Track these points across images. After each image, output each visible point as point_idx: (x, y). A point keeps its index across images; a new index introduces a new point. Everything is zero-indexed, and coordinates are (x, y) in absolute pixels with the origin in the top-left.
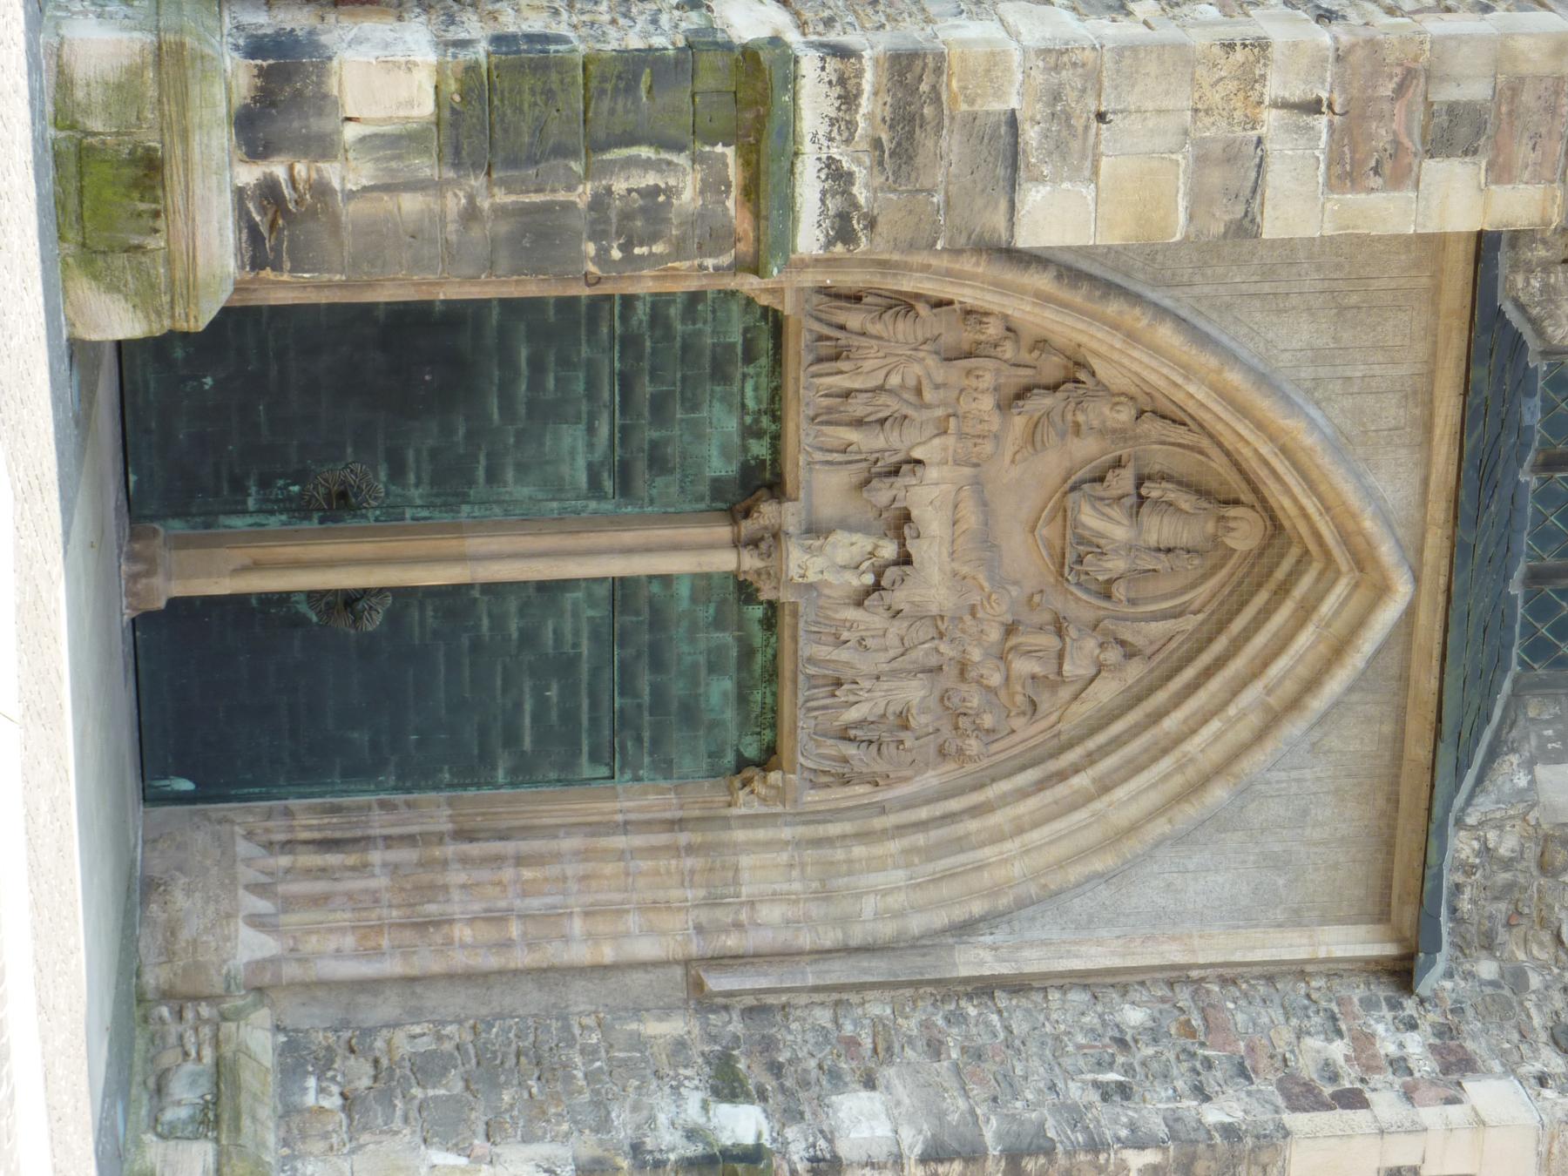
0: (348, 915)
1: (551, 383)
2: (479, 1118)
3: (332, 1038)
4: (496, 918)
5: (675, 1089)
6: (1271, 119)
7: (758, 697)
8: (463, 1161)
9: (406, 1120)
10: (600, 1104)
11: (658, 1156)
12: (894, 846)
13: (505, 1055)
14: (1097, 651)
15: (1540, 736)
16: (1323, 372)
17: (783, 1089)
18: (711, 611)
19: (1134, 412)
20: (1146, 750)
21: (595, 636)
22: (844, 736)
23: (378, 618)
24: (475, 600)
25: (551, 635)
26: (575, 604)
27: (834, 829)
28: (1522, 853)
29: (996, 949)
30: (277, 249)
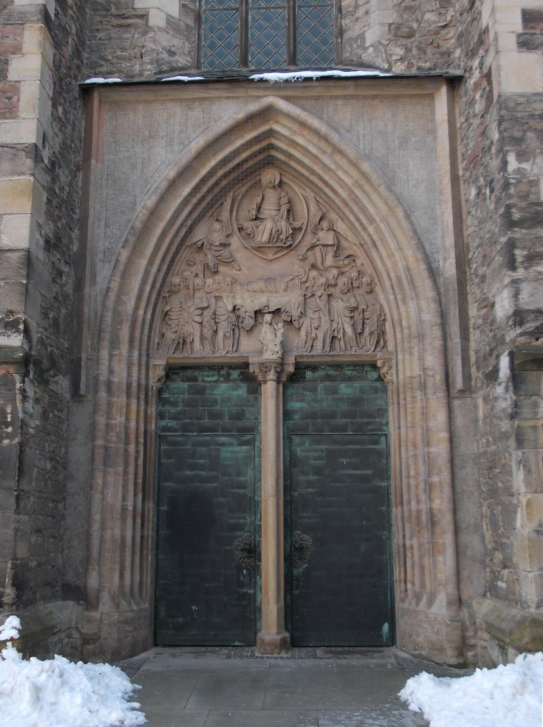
3: (488, 570)
12: (402, 309)
14: (324, 231)
15: (356, 49)
16: (176, 141)
18: (308, 393)
19: (216, 223)
21: (318, 443)
23: (306, 537)
24: (299, 494)
25: (317, 462)
26: (303, 451)
28: (402, 45)
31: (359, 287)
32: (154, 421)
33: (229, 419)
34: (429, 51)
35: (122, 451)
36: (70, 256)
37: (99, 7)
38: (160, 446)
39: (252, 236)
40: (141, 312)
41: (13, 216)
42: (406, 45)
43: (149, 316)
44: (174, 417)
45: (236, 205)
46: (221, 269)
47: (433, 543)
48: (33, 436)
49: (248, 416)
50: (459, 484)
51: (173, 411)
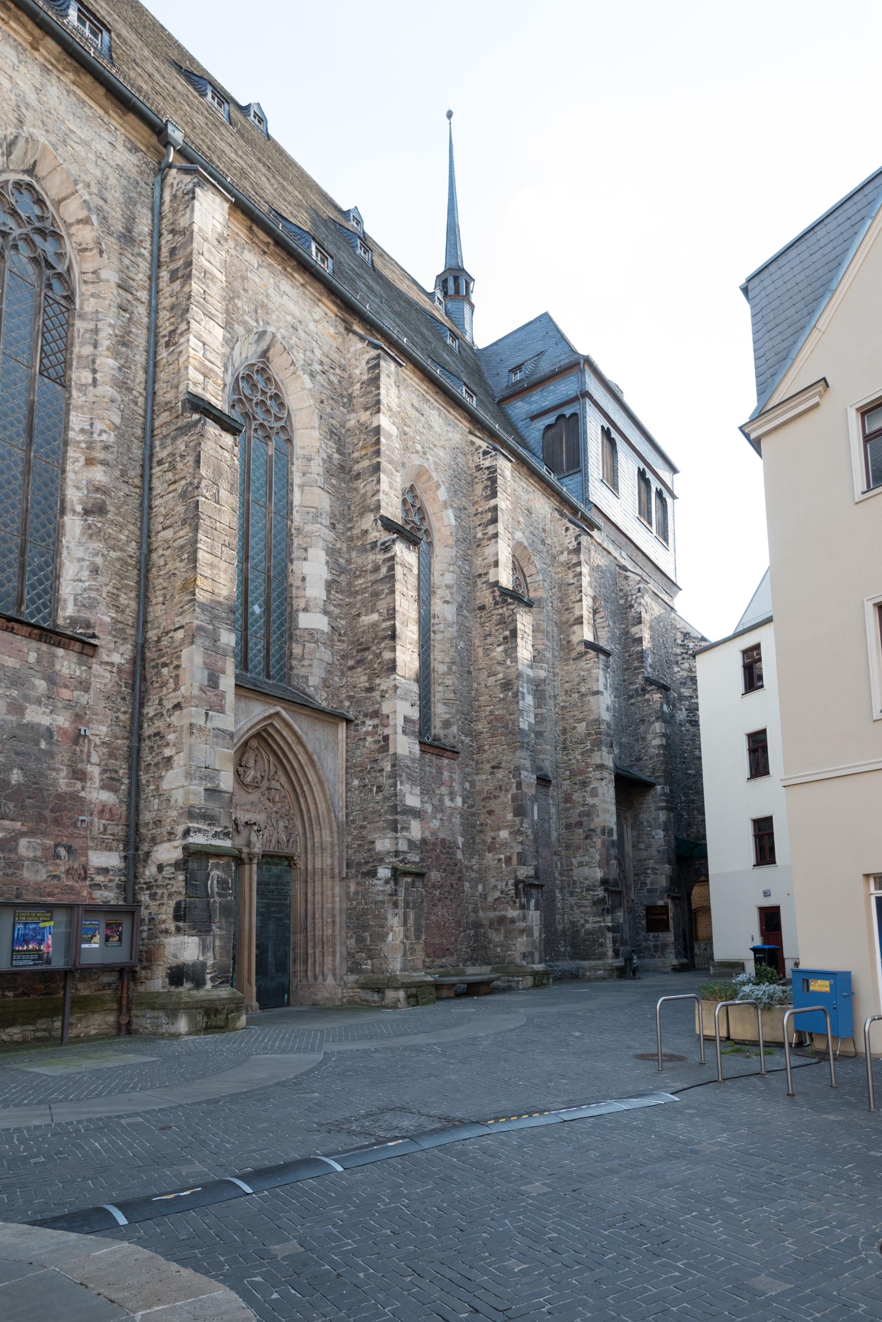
2: (377, 930)
6: (209, 725)
8: (391, 934)
10: (376, 903)
22: (288, 841)
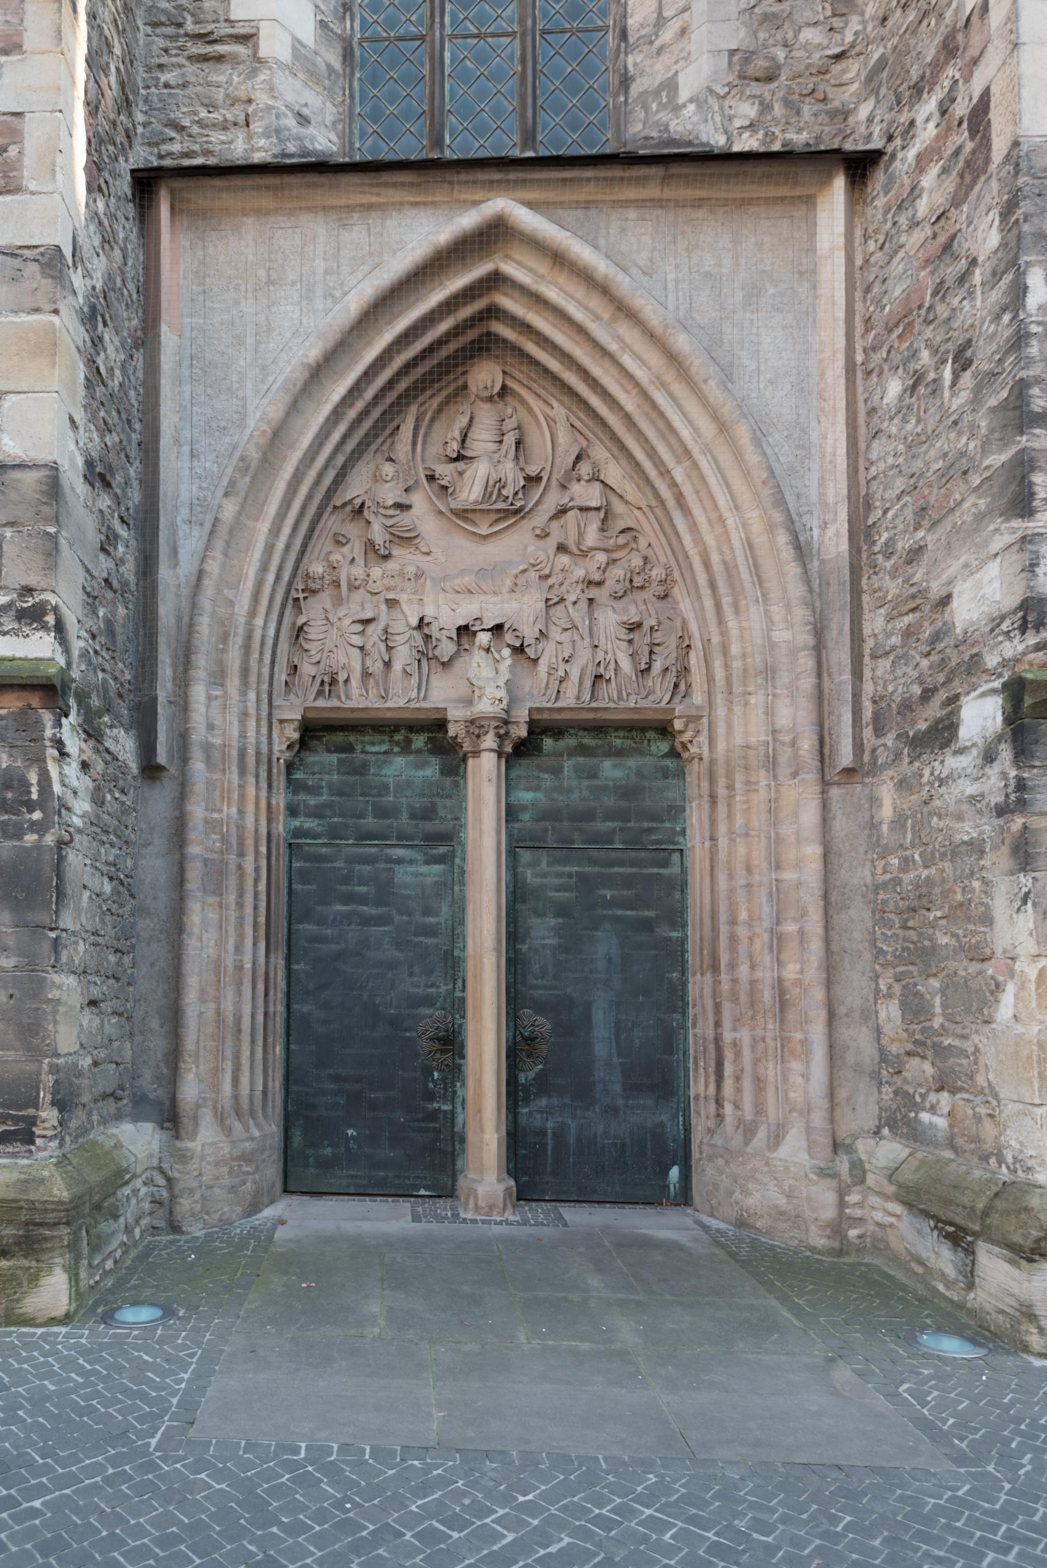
0: (771, 1065)
1: (363, 889)
3: (887, 1090)
4: (778, 943)
5: (942, 782)
7: (619, 741)
8: (1010, 988)
9: (964, 1037)
10: (954, 851)
11: (1010, 789)
12: (732, 623)
13: (906, 939)
14: (583, 483)
15: (657, 112)
16: (319, 292)
17: (948, 681)
18: (546, 776)
19: (388, 463)
20: (653, 422)
23: (541, 1020)
26: (535, 875)
27: (719, 673)
28: (755, 97)
29: (826, 524)
30: (17, 1119)
31: (642, 588)
32: (281, 818)
33: (410, 818)
34: (807, 110)
35: (232, 867)
36: (128, 509)
37: (163, 19)
38: (290, 862)
39: (450, 490)
40: (259, 621)
41: (22, 396)
42: (761, 96)
43: (271, 632)
44: (316, 814)
45: (422, 432)
46: (396, 551)
47: (782, 1039)
48: (80, 831)
49: (441, 813)
50: (836, 937)
51: (312, 802)
